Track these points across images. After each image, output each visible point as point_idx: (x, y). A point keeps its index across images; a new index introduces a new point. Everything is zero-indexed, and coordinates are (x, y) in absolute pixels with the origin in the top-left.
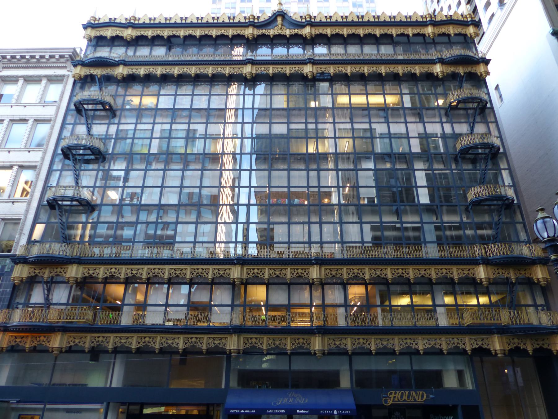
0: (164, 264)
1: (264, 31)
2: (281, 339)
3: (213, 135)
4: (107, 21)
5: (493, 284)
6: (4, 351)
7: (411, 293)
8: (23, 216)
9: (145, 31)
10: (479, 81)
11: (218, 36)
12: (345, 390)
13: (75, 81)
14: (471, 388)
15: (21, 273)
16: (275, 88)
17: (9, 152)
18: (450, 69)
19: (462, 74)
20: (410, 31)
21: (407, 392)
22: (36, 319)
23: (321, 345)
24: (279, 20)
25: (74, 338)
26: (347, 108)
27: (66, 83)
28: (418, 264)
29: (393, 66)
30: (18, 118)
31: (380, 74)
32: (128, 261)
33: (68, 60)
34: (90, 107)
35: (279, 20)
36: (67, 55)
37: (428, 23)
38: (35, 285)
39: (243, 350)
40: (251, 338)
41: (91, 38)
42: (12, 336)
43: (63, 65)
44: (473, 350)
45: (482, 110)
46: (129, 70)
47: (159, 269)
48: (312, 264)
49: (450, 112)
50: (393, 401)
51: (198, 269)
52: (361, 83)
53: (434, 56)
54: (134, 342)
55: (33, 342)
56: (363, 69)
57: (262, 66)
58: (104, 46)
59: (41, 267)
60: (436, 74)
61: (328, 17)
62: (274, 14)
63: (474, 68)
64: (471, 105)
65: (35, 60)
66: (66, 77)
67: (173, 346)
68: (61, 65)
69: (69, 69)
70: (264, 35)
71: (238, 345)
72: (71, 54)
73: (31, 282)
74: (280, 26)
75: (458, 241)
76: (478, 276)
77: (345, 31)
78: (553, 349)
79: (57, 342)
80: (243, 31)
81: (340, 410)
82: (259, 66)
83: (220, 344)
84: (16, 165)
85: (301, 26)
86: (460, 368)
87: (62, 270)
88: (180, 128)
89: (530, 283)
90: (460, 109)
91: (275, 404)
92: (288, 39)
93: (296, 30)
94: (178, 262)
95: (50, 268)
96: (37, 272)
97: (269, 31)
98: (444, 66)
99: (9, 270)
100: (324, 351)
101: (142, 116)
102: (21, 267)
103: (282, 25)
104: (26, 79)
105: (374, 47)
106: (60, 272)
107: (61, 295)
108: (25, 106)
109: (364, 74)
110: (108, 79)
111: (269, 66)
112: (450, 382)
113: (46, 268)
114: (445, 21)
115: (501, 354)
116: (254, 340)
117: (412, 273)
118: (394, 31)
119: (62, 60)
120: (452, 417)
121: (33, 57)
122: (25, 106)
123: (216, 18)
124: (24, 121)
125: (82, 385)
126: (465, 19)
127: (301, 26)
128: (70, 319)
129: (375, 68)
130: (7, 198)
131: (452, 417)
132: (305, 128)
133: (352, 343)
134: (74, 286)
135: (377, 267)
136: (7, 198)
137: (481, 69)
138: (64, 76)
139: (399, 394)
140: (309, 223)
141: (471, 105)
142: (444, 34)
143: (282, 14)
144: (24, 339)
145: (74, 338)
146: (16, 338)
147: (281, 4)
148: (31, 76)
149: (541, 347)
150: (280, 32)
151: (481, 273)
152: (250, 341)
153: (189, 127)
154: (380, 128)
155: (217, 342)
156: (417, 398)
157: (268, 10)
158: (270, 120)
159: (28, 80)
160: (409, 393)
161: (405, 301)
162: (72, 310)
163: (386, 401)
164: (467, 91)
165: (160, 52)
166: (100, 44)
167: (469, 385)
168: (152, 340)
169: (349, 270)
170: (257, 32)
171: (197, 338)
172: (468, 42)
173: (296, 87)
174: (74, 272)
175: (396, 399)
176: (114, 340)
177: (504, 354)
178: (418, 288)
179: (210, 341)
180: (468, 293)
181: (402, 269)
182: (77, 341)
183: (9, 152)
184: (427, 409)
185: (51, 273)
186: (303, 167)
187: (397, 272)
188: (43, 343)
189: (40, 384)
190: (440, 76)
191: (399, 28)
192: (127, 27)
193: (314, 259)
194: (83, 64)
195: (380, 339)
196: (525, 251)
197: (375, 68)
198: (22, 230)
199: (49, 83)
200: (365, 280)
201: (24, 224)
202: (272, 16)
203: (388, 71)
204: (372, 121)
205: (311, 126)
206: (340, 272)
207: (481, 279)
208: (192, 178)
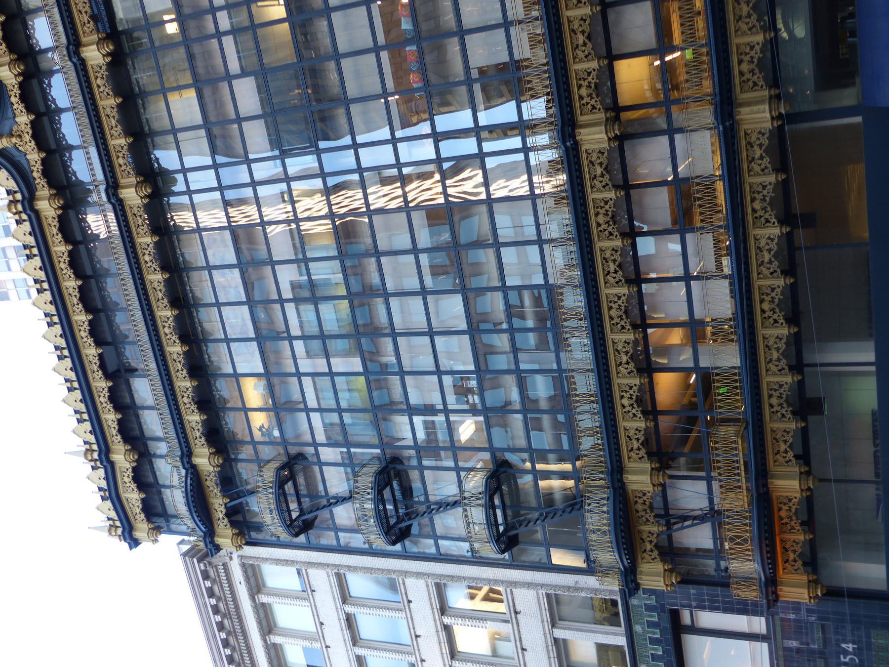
8: (429, 581)
11: (26, 108)
13: (248, 544)
15: (658, 575)
16: (156, 126)
22: (746, 531)
23: (762, 107)
30: (347, 633)
34: (293, 506)
36: (199, 567)
38: (675, 545)
41: (153, 529)
42: (784, 569)
48: (576, 145)
54: (775, 333)
55: (793, 528)
65: (226, 622)
70: (45, 173)
71: (761, 102)
72: (195, 560)
73: (671, 554)
74: (14, 140)
79: (788, 485)
82: (118, 170)
87: (641, 501)
93: (14, 100)
103: (11, 135)
104: (266, 631)
106: (644, 503)
107: (691, 494)
108: (322, 624)
110: (228, 481)
115: (816, 588)
116: (745, 67)
119: (212, 573)
124: (350, 622)
130: (510, 625)
134: (669, 472)
136: (510, 625)
138: (243, 566)
144: (778, 437)
148: (260, 623)
150: (27, 138)
152: (748, 76)
154: (287, 275)
159: (268, 626)
162: (719, 468)
165: (144, 389)
169: (603, 235)
170: (43, 190)
173: (143, 75)
174: (640, 478)
179: (757, 168)
182: (783, 447)
183: (417, 636)
185: (647, 520)
189: (879, 501)
194: (210, 533)
195: (749, 162)
198: (569, 588)
199: (264, 590)
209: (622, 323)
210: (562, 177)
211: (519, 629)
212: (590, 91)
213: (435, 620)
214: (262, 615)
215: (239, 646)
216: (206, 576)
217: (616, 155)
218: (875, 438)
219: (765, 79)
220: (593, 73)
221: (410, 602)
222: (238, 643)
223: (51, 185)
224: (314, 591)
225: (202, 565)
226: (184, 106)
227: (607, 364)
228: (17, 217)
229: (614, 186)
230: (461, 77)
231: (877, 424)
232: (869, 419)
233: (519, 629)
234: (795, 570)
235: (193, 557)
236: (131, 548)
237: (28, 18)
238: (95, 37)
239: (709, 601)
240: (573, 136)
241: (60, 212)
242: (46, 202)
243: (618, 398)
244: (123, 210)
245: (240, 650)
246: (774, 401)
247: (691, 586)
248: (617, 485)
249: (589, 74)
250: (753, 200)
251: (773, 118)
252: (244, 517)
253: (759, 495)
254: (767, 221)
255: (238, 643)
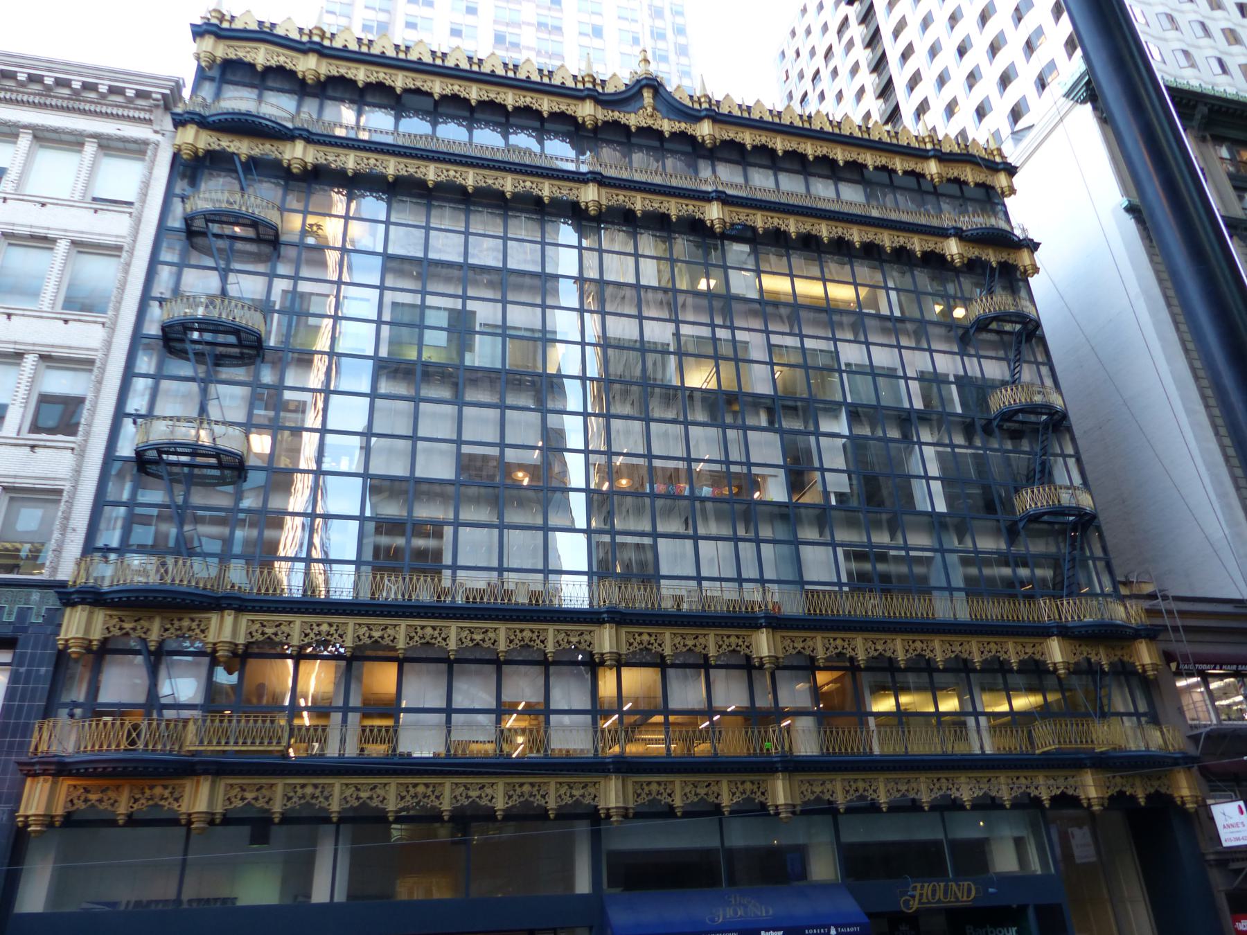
0: (447, 617)
1: (616, 114)
2: (375, 787)
3: (520, 329)
4: (254, 27)
5: (1074, 673)
6: (57, 824)
7: (897, 690)
9: (349, 68)
10: (1013, 277)
11: (519, 108)
12: (824, 887)
14: (1039, 872)
15: (87, 630)
16: (511, 222)
17: (9, 316)
18: (974, 252)
19: (994, 264)
20: (899, 165)
21: (942, 884)
22: (146, 745)
23: (621, 799)
24: (647, 95)
25: (243, 790)
26: (786, 305)
27: (153, 162)
28: (911, 631)
29: (874, 230)
30: (26, 231)
31: (502, 194)
32: (422, 610)
33: (157, 106)
35: (647, 95)
37: (704, 113)
38: (108, 657)
39: (224, 815)
40: (649, 783)
41: (214, 61)
42: (75, 786)
43: (142, 115)
44: (1054, 799)
45: (1024, 336)
46: (211, 140)
47: (434, 628)
48: (601, 622)
49: (966, 338)
50: (920, 903)
51: (522, 631)
52: (866, 262)
53: (947, 221)
56: (502, 182)
57: (449, 167)
58: (380, 106)
59: (138, 614)
60: (949, 258)
61: (439, 54)
62: (638, 81)
63: (1012, 256)
64: (1008, 327)
65: (66, 91)
66: (151, 147)
67: (101, 807)
68: (137, 114)
69: (158, 128)
70: (616, 124)
71: (625, 800)
72: (168, 92)
73: (100, 653)
74: (649, 110)
75: (1009, 590)
76: (757, 651)
77: (474, 93)
78: (1083, 797)
79: (199, 798)
80: (354, 71)
81: (843, 926)
82: (614, 191)
83: (583, 796)
84: (33, 352)
85: (693, 116)
86: (1017, 834)
87: (194, 625)
88: (441, 303)
89: (1126, 673)
90: (991, 331)
91: (712, 920)
92: (472, 110)
93: (683, 125)
94: (494, 614)
95: (163, 618)
96: (128, 626)
97: (627, 116)
98: (727, 209)
99: (41, 620)
100: (626, 809)
101: (279, 256)
102: (85, 614)
104: (40, 134)
105: (738, 169)
106: (190, 629)
107: (183, 687)
108: (43, 205)
109: (668, 216)
110: (257, 167)
111: (633, 194)
112: (1005, 861)
113: (150, 618)
114: (956, 154)
116: (654, 787)
117: (899, 649)
118: (870, 159)
119: (141, 102)
120: (1014, 929)
121: (65, 83)
122: (43, 205)
123: (365, 41)
125: (225, 900)
126: (922, 146)
127: (922, 155)
128: (261, 743)
129: (452, 173)
130: (14, 435)
131: (1014, 929)
132: (419, 302)
133: (506, 794)
135: (877, 636)
136: (14, 435)
137: (1024, 258)
138: (146, 143)
139: (927, 889)
140: (736, 539)
141: (1008, 327)
142: (956, 181)
143: (654, 85)
144: (264, 791)
145: (243, 790)
146: (86, 790)
147: (646, 61)
148: (55, 131)
149: (1063, 793)
150: (650, 122)
151: (1056, 652)
152: (646, 789)
153: (295, 285)
154: (486, 313)
155: (577, 793)
156: (960, 895)
157: (617, 70)
158: (544, 300)
159: (43, 137)
160: (946, 886)
161: (886, 704)
162: (204, 721)
163: (906, 903)
164: (1001, 301)
165: (851, 196)
166: (229, 77)
167: (1036, 867)
168: (172, 793)
169: (511, 633)
170: (603, 115)
171: (532, 785)
172: (991, 198)
173: (682, 246)
174: (225, 629)
175: (924, 900)
176: (342, 792)
177: (794, 813)
178: (911, 678)
179: (562, 791)
180: (991, 689)
181: (650, 635)
183: (9, 316)
184: (957, 917)
186: (446, 394)
187: (519, 635)
188: (162, 803)
189: (114, 904)
190: (718, 227)
191: (878, 153)
192: (305, 52)
193: (607, 612)
195: (568, 784)
196: (1118, 613)
197: (776, 221)
199: (101, 153)
200: (546, 655)
201: (70, 504)
202: (634, 86)
203: (557, 194)
204: (510, 298)
205: (722, 334)
206: (491, 635)
207: (761, 658)
208: (480, 426)
209: (417, 638)
210: (298, 594)
211: (6, 444)
212: (324, 634)
213: (34, 345)
214: (64, 137)
215: (24, 93)
216: (140, 94)
217: (536, 657)
218: (199, 901)
219: (292, 809)
220: (444, 643)
221: (66, 321)
222: (29, 94)
223: (606, 123)
224: (96, 211)
225: (159, 96)
226: (889, 303)
227: (374, 614)
228: (307, 31)
229: (250, 643)
230: (507, 520)
231: (218, 905)
232: (224, 893)
233: (6, 444)
234: (71, 801)
235: (172, 91)
236: (192, 25)
237: (355, 107)
238: (604, 202)
239: (24, 690)
240: (83, 602)
241: (300, 76)
242: (209, 49)
243: (650, 631)
244: (578, 181)
245: (18, 92)
246: (309, 790)
247: (51, 669)
248: (224, 603)
249: (542, 642)
250: (532, 785)
251: (608, 809)
252: (207, 168)
253: (193, 764)
254: (510, 797)
255: (29, 94)
